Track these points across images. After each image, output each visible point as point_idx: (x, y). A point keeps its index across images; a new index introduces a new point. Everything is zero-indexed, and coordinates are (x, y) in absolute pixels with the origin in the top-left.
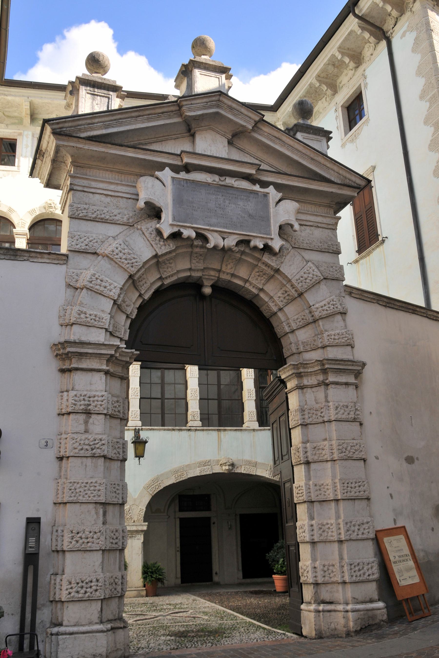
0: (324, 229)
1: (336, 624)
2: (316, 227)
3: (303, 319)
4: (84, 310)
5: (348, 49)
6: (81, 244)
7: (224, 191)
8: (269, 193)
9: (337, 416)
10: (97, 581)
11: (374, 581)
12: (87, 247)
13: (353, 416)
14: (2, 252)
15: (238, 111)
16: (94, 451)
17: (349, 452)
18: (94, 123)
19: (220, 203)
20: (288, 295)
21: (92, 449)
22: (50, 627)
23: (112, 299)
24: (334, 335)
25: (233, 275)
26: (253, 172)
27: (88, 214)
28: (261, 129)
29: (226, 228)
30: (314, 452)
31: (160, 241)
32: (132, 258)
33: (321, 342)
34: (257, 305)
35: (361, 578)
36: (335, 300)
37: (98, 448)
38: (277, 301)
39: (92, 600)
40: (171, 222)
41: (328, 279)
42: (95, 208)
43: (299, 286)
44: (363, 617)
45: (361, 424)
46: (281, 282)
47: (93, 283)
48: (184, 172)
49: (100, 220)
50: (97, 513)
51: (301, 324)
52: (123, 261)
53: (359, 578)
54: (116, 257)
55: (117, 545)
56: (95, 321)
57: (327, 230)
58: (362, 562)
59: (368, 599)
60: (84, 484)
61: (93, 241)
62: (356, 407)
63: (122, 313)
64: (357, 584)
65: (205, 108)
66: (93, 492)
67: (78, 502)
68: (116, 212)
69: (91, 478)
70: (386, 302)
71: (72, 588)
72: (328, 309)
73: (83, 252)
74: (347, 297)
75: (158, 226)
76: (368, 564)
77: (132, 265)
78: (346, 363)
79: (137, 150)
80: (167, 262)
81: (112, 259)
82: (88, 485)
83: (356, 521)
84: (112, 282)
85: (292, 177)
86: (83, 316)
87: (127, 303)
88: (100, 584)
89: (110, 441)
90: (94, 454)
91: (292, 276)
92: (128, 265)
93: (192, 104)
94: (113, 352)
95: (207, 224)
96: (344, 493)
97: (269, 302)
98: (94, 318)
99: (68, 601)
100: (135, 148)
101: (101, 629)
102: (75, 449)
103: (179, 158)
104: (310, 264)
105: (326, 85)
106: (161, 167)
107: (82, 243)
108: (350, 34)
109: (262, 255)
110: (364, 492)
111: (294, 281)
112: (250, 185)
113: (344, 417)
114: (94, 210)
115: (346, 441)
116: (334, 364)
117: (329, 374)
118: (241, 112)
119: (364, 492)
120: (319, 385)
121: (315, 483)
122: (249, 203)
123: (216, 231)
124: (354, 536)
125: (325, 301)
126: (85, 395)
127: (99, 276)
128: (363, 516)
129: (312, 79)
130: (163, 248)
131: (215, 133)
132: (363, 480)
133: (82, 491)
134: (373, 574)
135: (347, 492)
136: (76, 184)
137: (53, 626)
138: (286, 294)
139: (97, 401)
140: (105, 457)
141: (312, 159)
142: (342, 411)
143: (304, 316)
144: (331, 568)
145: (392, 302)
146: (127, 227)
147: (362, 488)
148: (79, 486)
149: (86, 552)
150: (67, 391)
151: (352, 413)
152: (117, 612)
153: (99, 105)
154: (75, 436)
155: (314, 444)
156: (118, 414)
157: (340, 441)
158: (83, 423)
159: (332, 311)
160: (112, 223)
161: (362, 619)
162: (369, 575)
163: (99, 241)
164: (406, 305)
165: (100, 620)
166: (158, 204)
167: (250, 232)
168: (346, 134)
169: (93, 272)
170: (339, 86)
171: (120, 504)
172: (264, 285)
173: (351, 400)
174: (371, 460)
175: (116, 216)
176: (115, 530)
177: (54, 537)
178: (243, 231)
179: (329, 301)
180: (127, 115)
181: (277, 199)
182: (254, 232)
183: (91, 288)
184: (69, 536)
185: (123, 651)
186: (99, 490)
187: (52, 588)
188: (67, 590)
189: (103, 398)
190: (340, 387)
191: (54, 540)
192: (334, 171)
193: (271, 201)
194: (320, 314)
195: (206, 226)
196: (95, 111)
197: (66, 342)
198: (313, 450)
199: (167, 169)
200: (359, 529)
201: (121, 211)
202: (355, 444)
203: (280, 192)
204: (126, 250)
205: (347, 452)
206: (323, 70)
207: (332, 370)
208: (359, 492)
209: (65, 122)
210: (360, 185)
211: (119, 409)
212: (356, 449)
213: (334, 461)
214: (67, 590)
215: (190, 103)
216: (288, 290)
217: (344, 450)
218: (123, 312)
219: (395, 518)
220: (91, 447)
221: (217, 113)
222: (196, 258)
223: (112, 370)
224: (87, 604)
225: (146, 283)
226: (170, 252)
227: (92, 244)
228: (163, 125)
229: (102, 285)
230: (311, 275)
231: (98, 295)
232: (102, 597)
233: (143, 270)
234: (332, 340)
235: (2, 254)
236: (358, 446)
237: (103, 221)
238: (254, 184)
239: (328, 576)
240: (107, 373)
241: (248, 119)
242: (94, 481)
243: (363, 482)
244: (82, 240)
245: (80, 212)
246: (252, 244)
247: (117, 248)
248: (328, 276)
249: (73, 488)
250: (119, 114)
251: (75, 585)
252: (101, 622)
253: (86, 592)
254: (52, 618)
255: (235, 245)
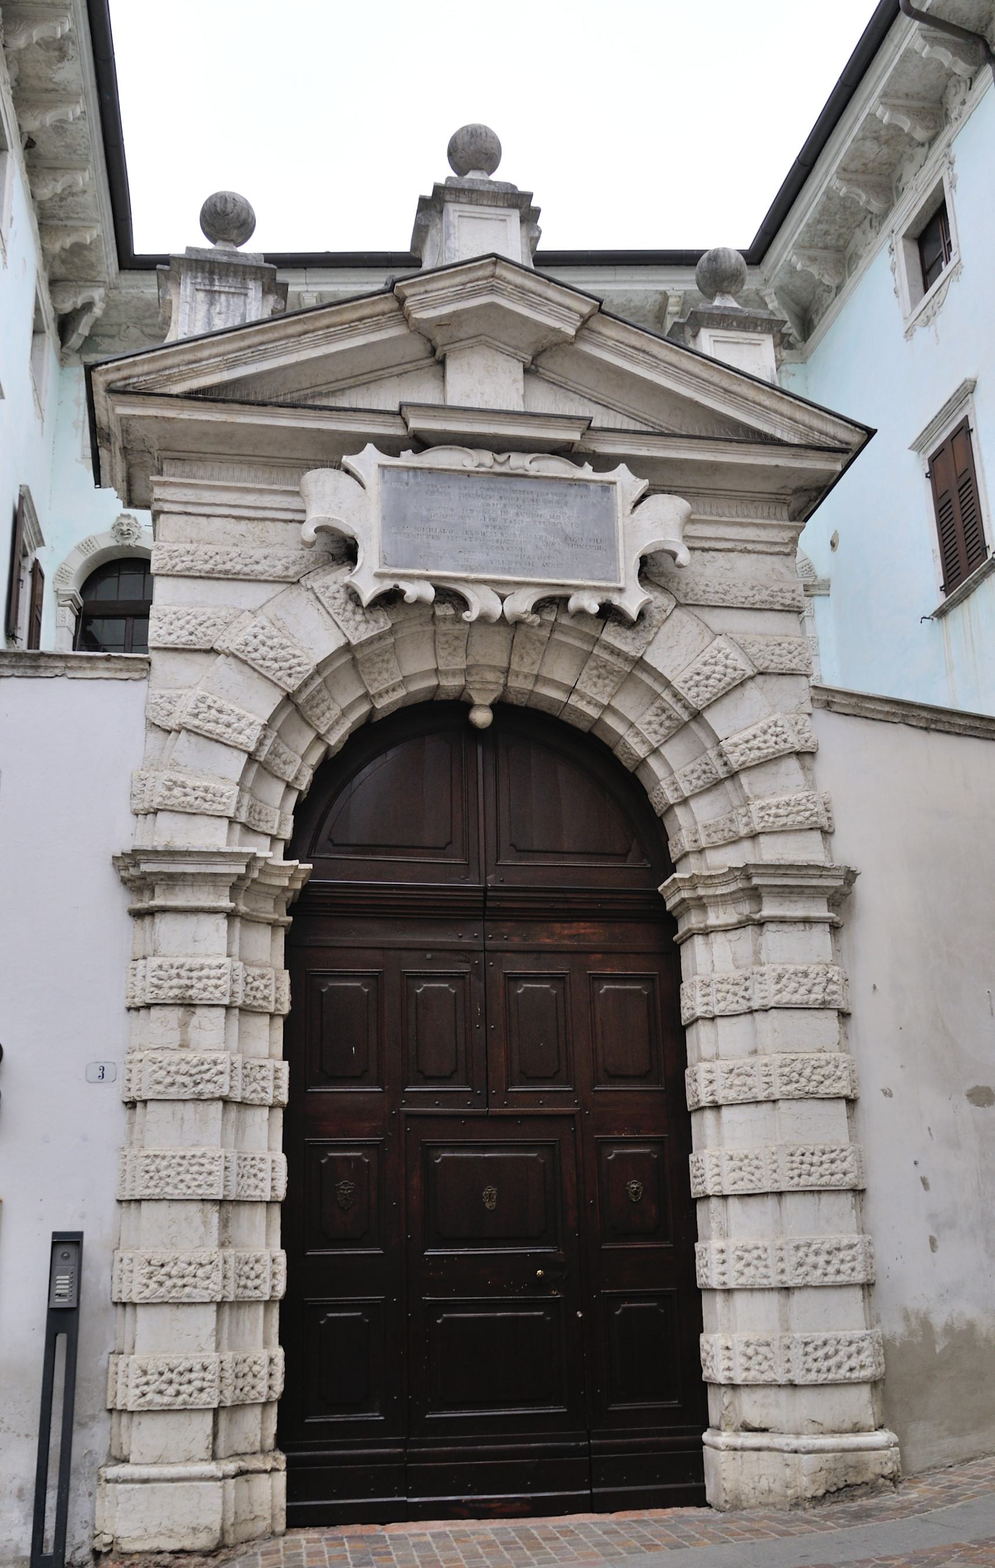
0: (761, 556)
1: (771, 1480)
2: (741, 551)
3: (704, 772)
4: (180, 778)
5: (907, 95)
6: (180, 632)
7: (504, 486)
8: (614, 483)
9: (779, 996)
10: (205, 1369)
11: (864, 1382)
12: (193, 637)
13: (820, 997)
14: (6, 662)
15: (540, 296)
16: (200, 1086)
17: (809, 1081)
18: (201, 360)
19: (493, 515)
20: (669, 718)
21: (196, 1084)
22: (106, 1465)
23: (245, 751)
24: (778, 807)
25: (537, 678)
26: (575, 436)
27: (194, 564)
28: (600, 333)
29: (508, 571)
30: (728, 1082)
31: (354, 613)
32: (289, 657)
33: (747, 825)
34: (606, 742)
35: (831, 1376)
36: (780, 723)
37: (209, 1081)
38: (645, 733)
39: (191, 1409)
40: (377, 569)
41: (770, 674)
42: (211, 549)
43: (690, 696)
44: (832, 1466)
45: (844, 1015)
46: (650, 689)
47: (200, 717)
48: (410, 451)
49: (222, 576)
50: (205, 1223)
51: (701, 783)
52: (267, 663)
53: (824, 1376)
54: (254, 655)
55: (257, 1291)
56: (205, 801)
57: (769, 558)
58: (835, 1339)
59: (847, 1425)
60: (178, 1160)
61: (205, 624)
62: (829, 975)
63: (275, 780)
64: (822, 1390)
65: (459, 297)
66: (197, 1176)
67: (164, 1199)
68: (258, 554)
69: (193, 1145)
70: (927, 719)
71: (147, 1383)
72: (762, 745)
73: (183, 650)
74: (821, 715)
75: (347, 579)
76: (851, 1343)
77: (289, 672)
78: (804, 872)
79: (300, 411)
80: (376, 659)
81: (245, 662)
82: (185, 1162)
83: (823, 1243)
84: (243, 712)
85: (675, 439)
86: (177, 791)
87: (284, 757)
88: (209, 1377)
89: (238, 1065)
90: (200, 1094)
91: (675, 673)
92: (279, 674)
93: (426, 292)
94: (242, 870)
95: (462, 566)
96: (792, 1178)
97: (626, 737)
98: (203, 794)
99: (140, 1412)
100: (294, 406)
101: (210, 1474)
102: (159, 1083)
103: (399, 420)
104: (720, 642)
105: (863, 190)
106: (356, 444)
107: (182, 628)
108: (904, 59)
109: (601, 627)
110: (845, 1174)
111: (677, 684)
112: (568, 468)
113: (797, 998)
114: (209, 554)
115: (801, 1056)
116: (774, 875)
117: (764, 899)
118: (546, 299)
119: (845, 1174)
120: (740, 925)
121: (731, 1153)
122: (565, 509)
123: (485, 582)
124: (815, 1277)
125: (756, 727)
126: (182, 966)
127: (215, 702)
128: (841, 1232)
129: (828, 178)
130: (362, 627)
131: (493, 351)
132: (843, 1147)
133: (173, 1174)
134: (862, 1367)
135: (800, 1176)
136: (169, 498)
137: (114, 1462)
138: (664, 717)
139: (208, 978)
140: (226, 1101)
141: (726, 391)
142: (793, 985)
143: (707, 764)
144: (763, 1350)
145: (944, 718)
146: (284, 586)
147: (838, 1166)
148: (165, 1163)
149: (180, 1306)
150: (144, 958)
151: (818, 989)
152: (259, 1437)
153: (223, 316)
154: (158, 1056)
155: (728, 1062)
156: (265, 1004)
157: (785, 1056)
158: (176, 1026)
159: (771, 750)
160: (250, 581)
161: (829, 1471)
162: (851, 1370)
163: (219, 621)
164: (985, 723)
165: (210, 1453)
166: (347, 531)
167: (567, 578)
168: (914, 302)
169: (202, 693)
170: (897, 187)
171: (267, 1202)
172: (613, 696)
173: (818, 960)
174: (870, 1099)
175: (257, 563)
176: (252, 1259)
177: (117, 1272)
178: (549, 577)
179: (766, 727)
180: (276, 335)
181: (636, 495)
182: (577, 578)
183: (195, 730)
184: (142, 1271)
185: (269, 1521)
186: (210, 1174)
187: (110, 1384)
188: (137, 1386)
189: (222, 971)
190: (791, 928)
191: (116, 1280)
192: (782, 415)
193: (619, 501)
194: (742, 759)
195: (461, 571)
196: (215, 329)
197: (135, 852)
198: (726, 1076)
199: (370, 447)
200: (828, 1262)
201: (271, 551)
202: (823, 1063)
203: (643, 478)
204: (275, 640)
205: (803, 1081)
206: (852, 156)
207: (769, 890)
208: (832, 1174)
209: (134, 364)
210: (847, 443)
211: (266, 992)
212: (827, 1073)
213: (774, 1101)
214: (137, 1386)
215: (422, 289)
216: (667, 706)
217: (795, 1076)
218: (277, 777)
219: (935, 1235)
220: (194, 1078)
221: (493, 305)
222: (446, 646)
223: (243, 908)
224: (181, 1418)
225: (329, 709)
226: (380, 637)
227: (204, 630)
228: (364, 345)
229: (221, 721)
230: (719, 668)
231: (213, 743)
232: (215, 1405)
233: (319, 680)
234: (771, 819)
235: (7, 666)
236: (830, 1066)
237: (230, 576)
238: (580, 465)
239: (757, 1367)
240: (231, 915)
241: (565, 312)
242: (199, 1154)
243: (842, 1150)
244: (182, 622)
245: (177, 560)
246: (572, 604)
247: (255, 637)
248: (767, 668)
249: (152, 1168)
250: (258, 332)
251: (156, 1376)
252: (214, 1457)
253: (178, 1393)
254: (110, 1446)
255: (530, 609)
